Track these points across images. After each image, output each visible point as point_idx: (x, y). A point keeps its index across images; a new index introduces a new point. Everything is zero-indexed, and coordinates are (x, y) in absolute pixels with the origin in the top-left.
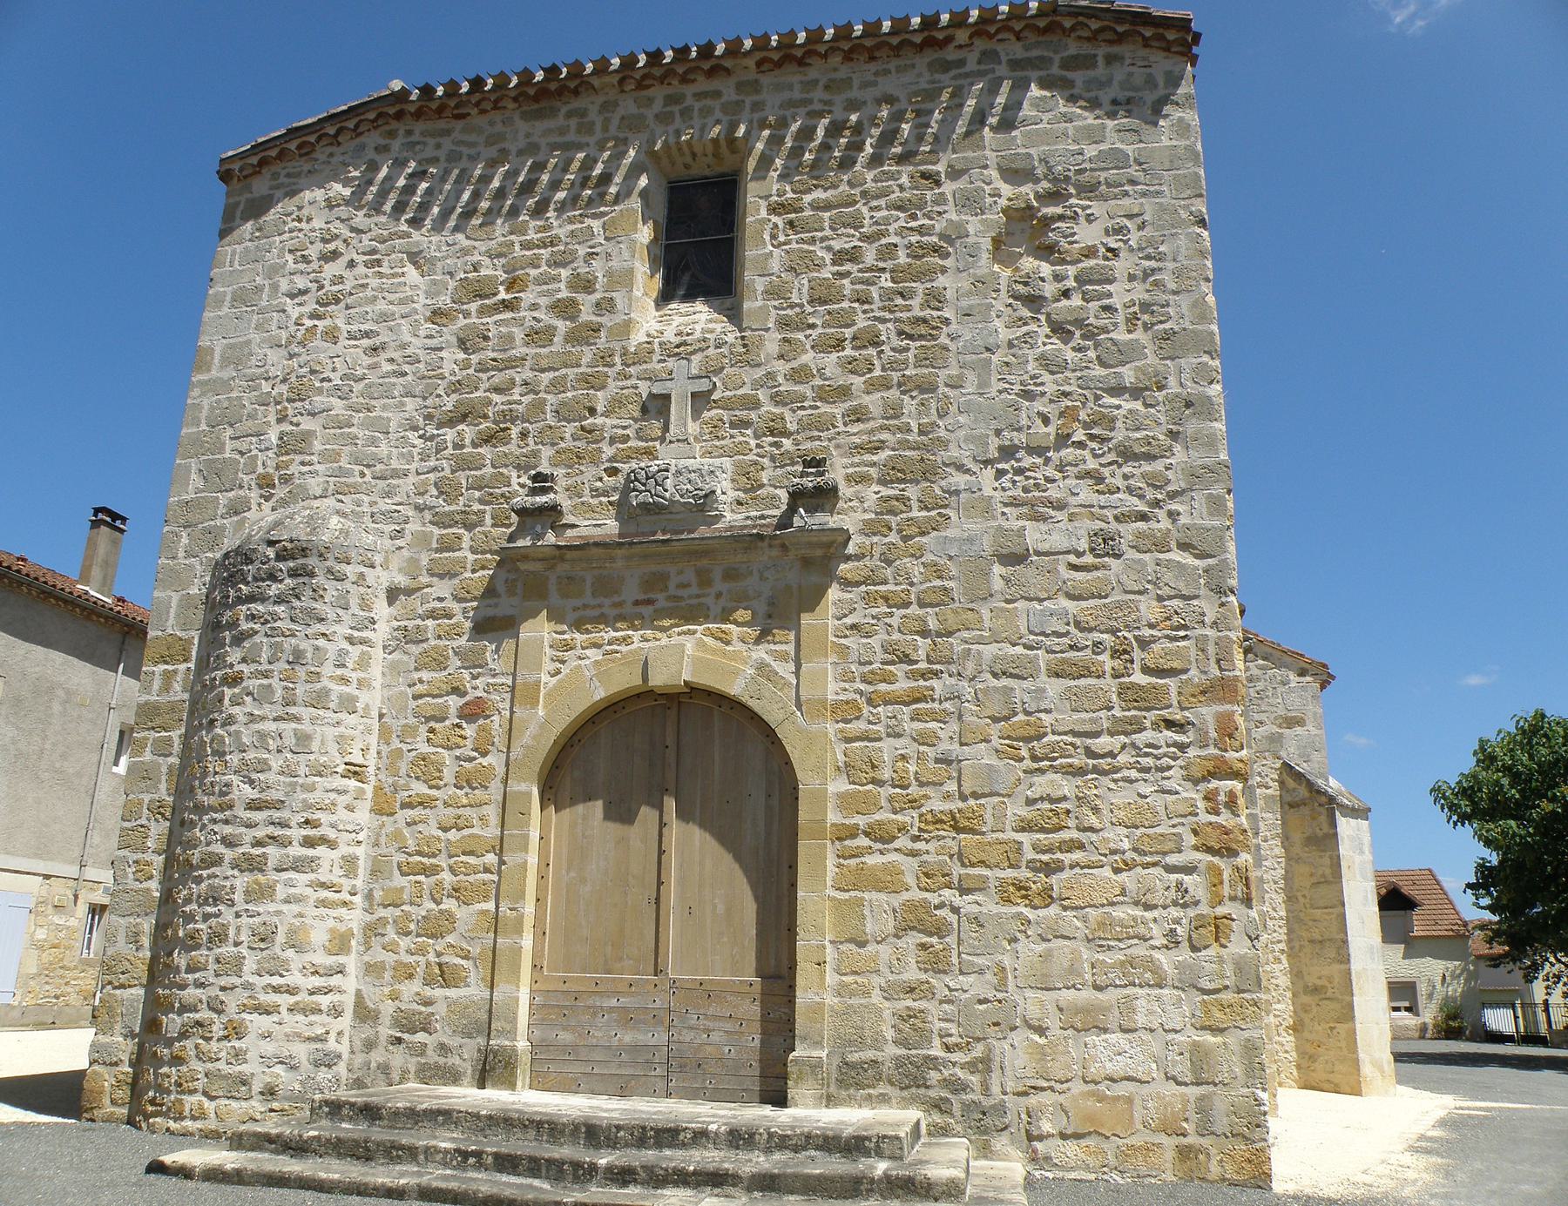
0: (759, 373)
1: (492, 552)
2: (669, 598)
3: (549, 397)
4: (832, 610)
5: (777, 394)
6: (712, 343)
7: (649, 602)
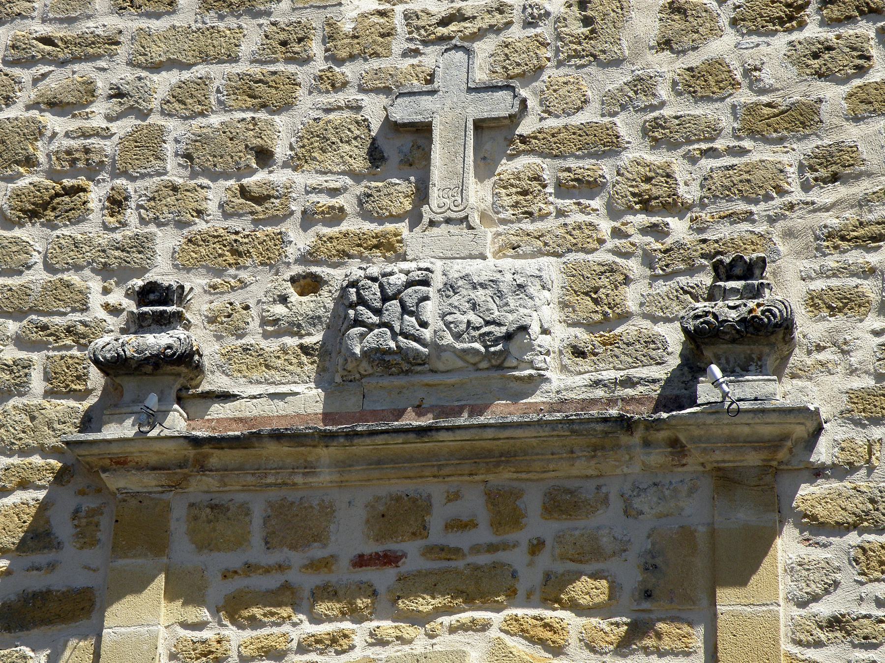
0: (618, 78)
1: (43, 450)
2: (431, 551)
3: (171, 124)
4: (785, 585)
5: (657, 124)
6: (517, 16)
7: (389, 559)
